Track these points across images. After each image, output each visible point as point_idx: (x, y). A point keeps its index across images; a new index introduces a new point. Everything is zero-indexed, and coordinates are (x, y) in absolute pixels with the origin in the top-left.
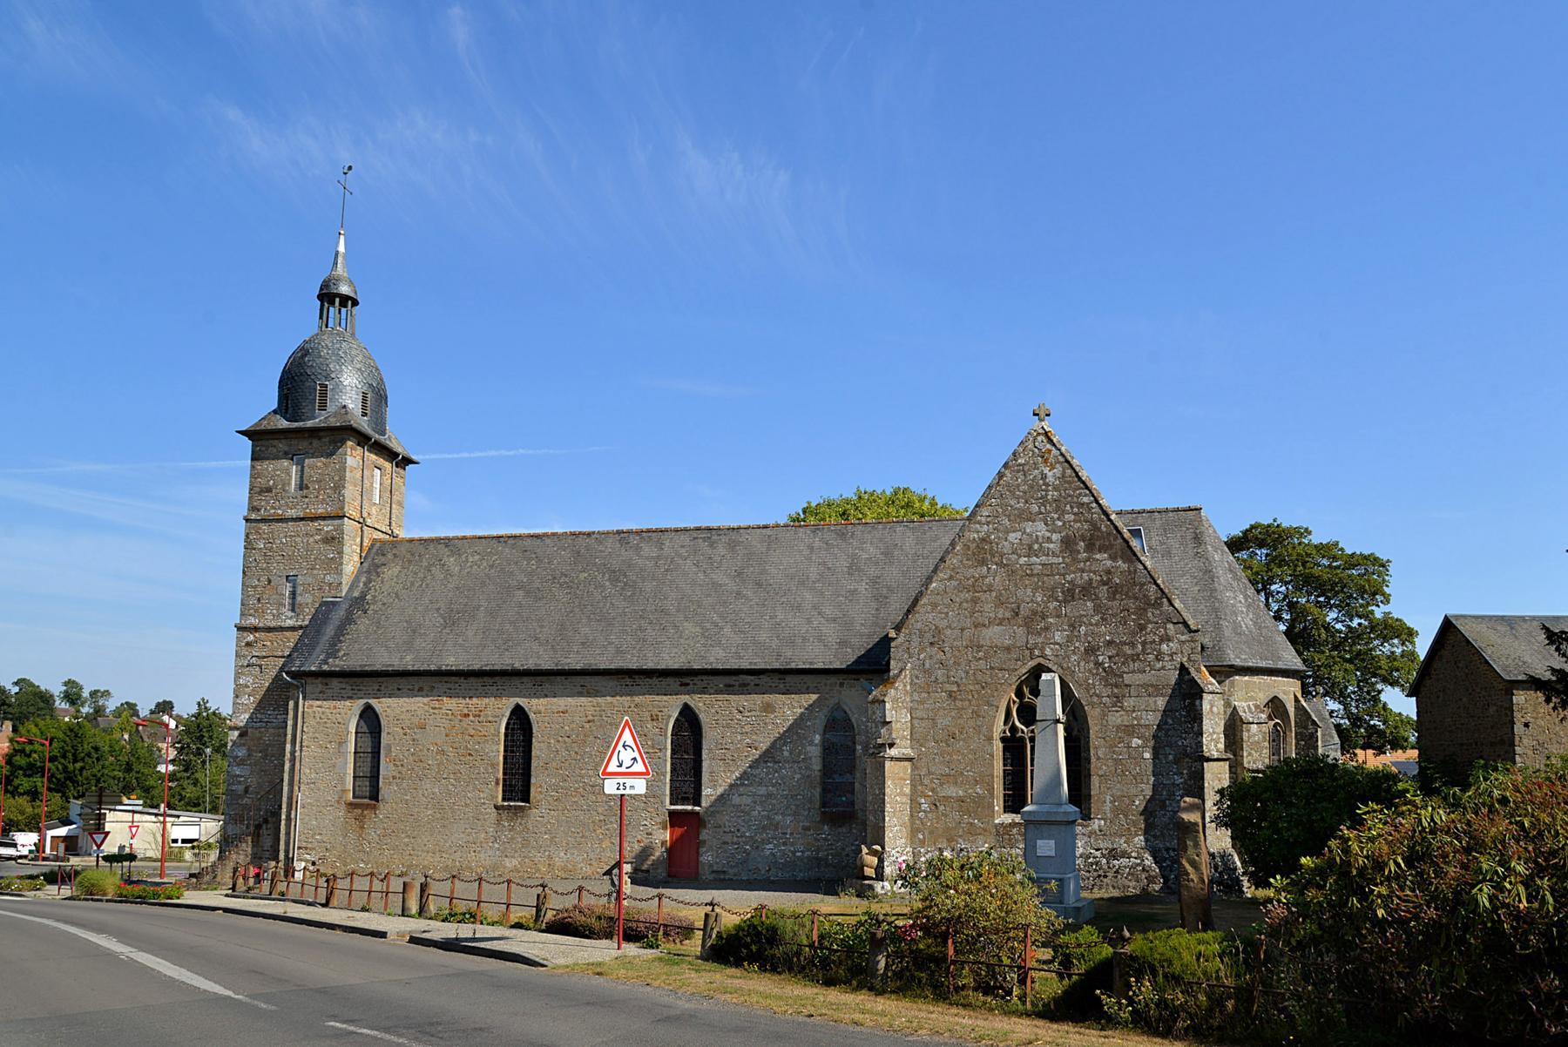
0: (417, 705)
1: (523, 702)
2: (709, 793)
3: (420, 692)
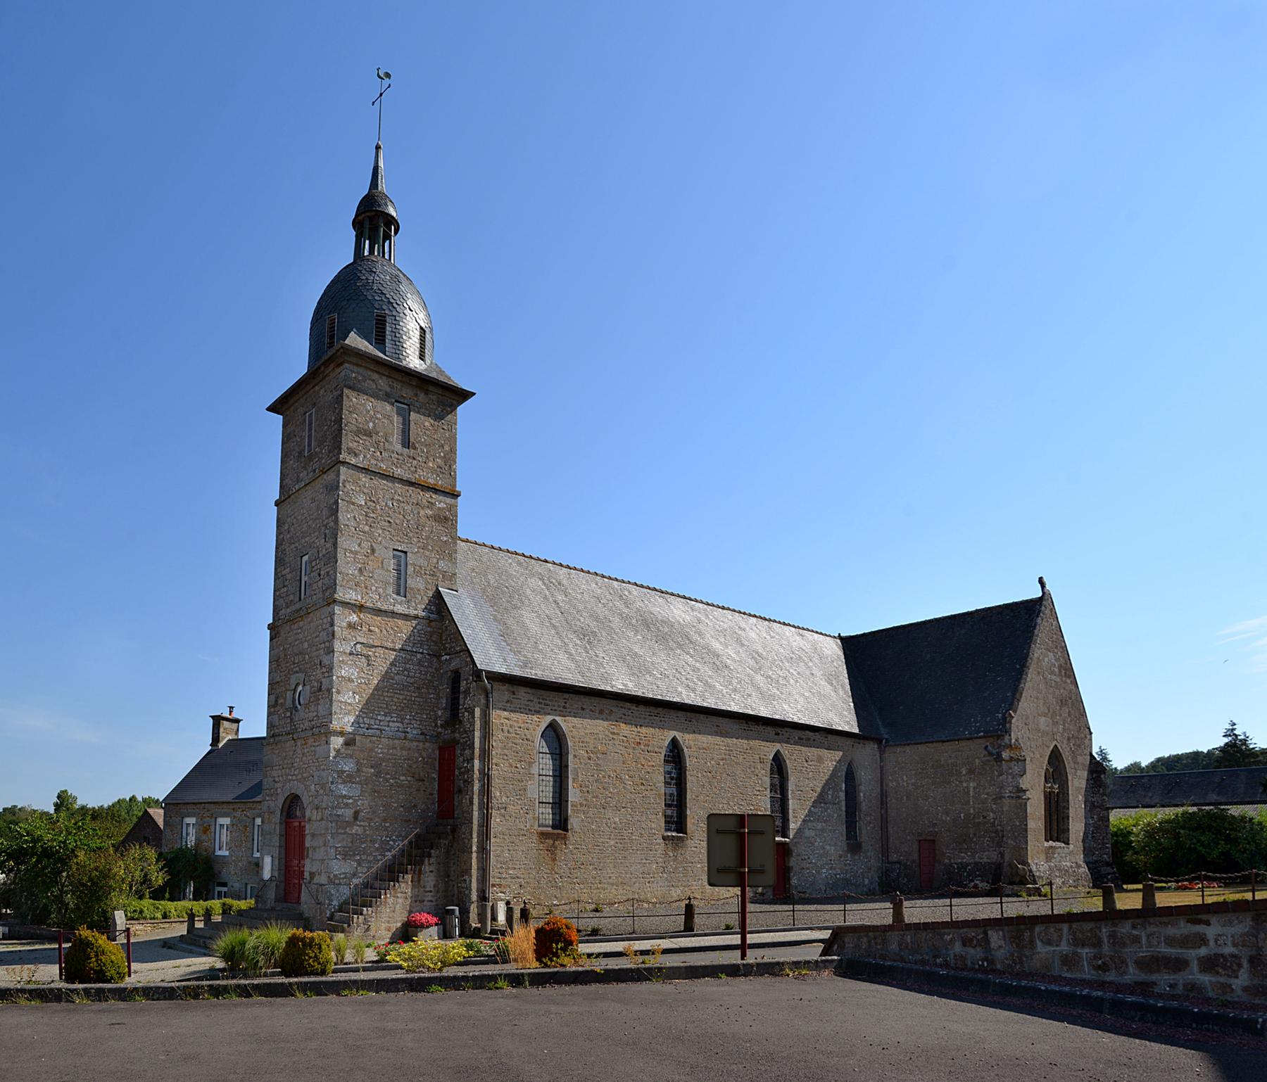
0: (599, 727)
1: (679, 735)
2: (793, 826)
3: (601, 714)
